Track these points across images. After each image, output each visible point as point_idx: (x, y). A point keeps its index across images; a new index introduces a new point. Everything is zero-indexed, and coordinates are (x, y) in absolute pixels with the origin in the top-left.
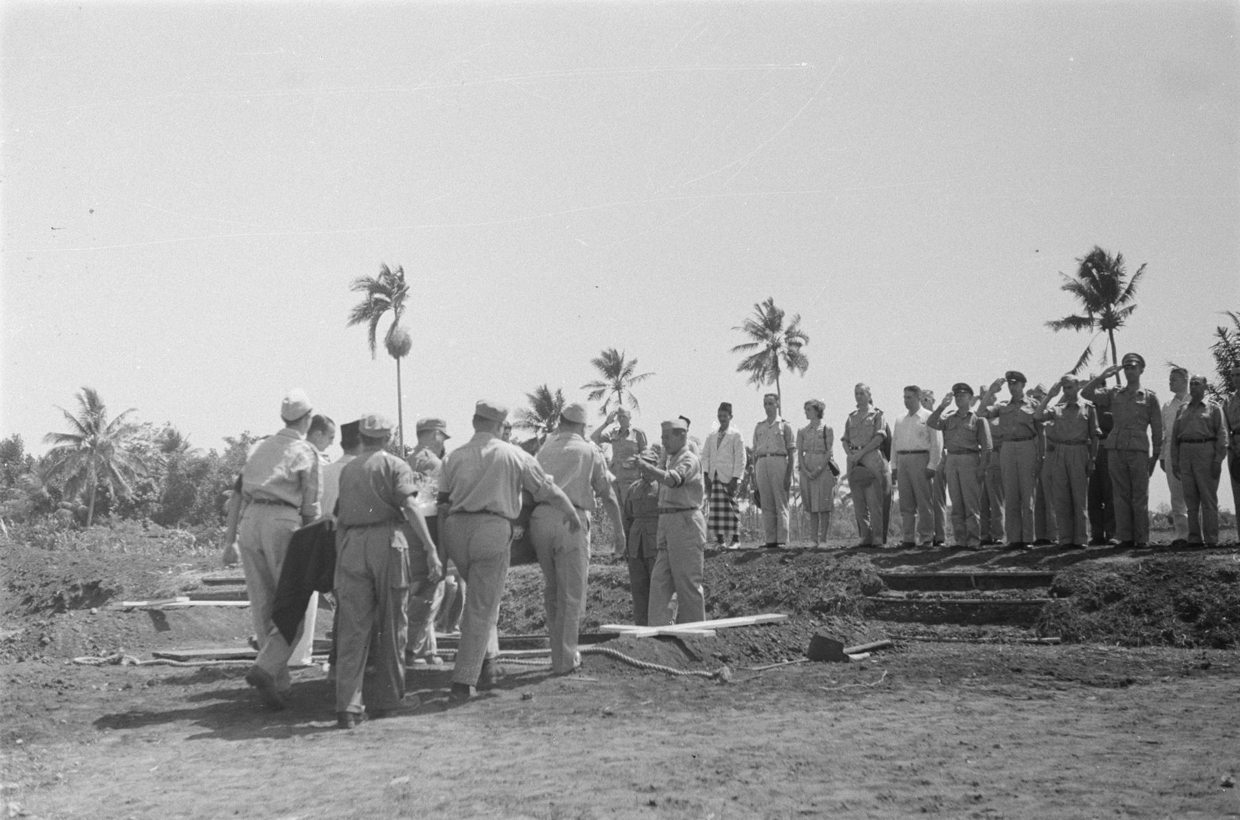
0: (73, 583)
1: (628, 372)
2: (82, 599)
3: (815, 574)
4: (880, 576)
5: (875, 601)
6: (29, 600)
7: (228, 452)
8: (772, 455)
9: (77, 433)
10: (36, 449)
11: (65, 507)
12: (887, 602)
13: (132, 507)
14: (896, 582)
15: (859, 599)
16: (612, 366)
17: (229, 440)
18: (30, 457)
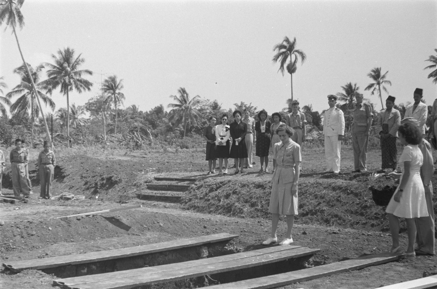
0: (103, 177)
1: (384, 77)
2: (105, 184)
6: (86, 183)
9: (178, 103)
10: (167, 110)
11: (177, 130)
13: (200, 130)
16: (377, 75)
18: (166, 112)
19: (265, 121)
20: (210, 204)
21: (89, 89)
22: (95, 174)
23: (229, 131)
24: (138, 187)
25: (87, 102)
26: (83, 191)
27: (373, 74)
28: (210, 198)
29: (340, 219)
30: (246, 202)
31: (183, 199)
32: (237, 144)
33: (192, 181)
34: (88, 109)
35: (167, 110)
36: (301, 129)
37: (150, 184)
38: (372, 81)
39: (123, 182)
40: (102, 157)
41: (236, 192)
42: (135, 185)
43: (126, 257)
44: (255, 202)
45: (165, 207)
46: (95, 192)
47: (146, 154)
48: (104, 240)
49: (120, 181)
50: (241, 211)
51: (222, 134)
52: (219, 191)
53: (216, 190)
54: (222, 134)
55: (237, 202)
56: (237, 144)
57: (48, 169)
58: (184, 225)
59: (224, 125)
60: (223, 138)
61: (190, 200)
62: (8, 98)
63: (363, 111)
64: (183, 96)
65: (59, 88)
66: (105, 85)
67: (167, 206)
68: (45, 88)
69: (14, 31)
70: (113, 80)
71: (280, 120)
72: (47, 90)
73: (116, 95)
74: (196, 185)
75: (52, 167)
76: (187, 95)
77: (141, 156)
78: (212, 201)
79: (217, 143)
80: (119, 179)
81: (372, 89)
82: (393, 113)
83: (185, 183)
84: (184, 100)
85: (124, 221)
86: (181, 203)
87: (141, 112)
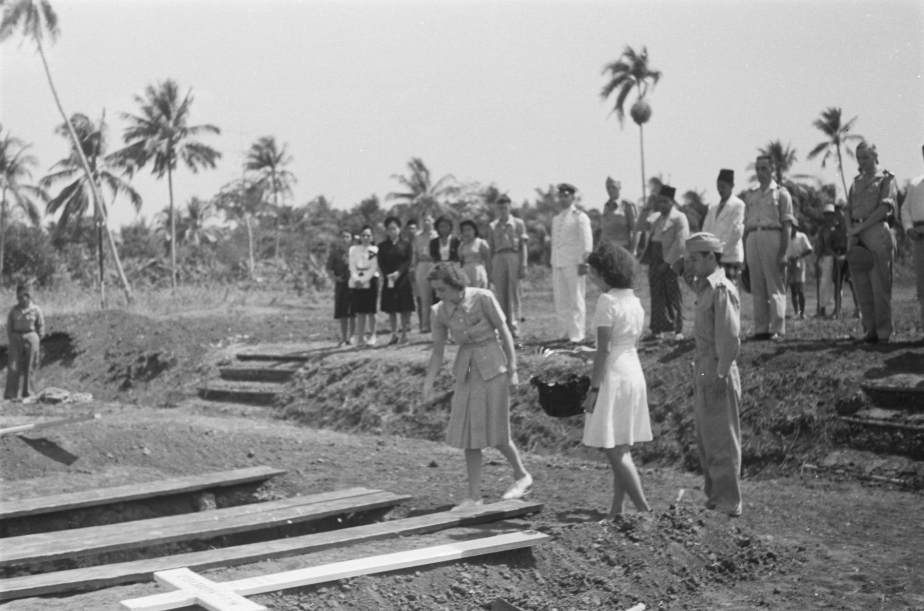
1: (846, 128)
2: (146, 370)
3: (785, 382)
4: (865, 389)
5: (851, 423)
6: (112, 369)
7: (538, 203)
8: (763, 228)
9: (408, 190)
12: (866, 426)
14: (882, 398)
15: (829, 420)
16: (832, 123)
17: (539, 191)
19: (450, 237)
20: (324, 407)
21: (213, 165)
22: (131, 350)
23: (375, 260)
24: (204, 374)
25: (217, 192)
26: (106, 383)
27: (825, 120)
28: (326, 395)
29: (546, 435)
30: (390, 402)
31: (278, 399)
32: (391, 284)
33: (300, 359)
34: (219, 207)
35: (386, 205)
36: (515, 252)
37: (227, 367)
38: (824, 137)
39: (180, 365)
40: (219, 310)
41: (375, 382)
42: (199, 370)
43: (24, 514)
44: (405, 403)
45: (243, 415)
46: (126, 386)
47: (315, 302)
48: (13, 483)
49: (174, 362)
50: (377, 421)
51: (361, 265)
52: (345, 381)
53: (341, 379)
54: (362, 264)
55: (374, 402)
56: (391, 284)
57: (27, 341)
58: (199, 452)
59: (366, 246)
60: (364, 272)
61: (291, 400)
62: (42, 187)
63: (619, 216)
64: (417, 176)
65: (150, 165)
66: (252, 156)
67: (246, 413)
68: (122, 163)
69: (40, 48)
70: (269, 144)
71: (477, 235)
72: (125, 169)
73: (277, 176)
74: (307, 369)
75: (34, 338)
76: (427, 173)
77: (304, 306)
78: (330, 403)
79: (351, 284)
80: (172, 360)
81: (822, 154)
82: (672, 220)
83: (284, 367)
84: (420, 185)
85: (68, 445)
86: (274, 407)
87: (336, 211)
